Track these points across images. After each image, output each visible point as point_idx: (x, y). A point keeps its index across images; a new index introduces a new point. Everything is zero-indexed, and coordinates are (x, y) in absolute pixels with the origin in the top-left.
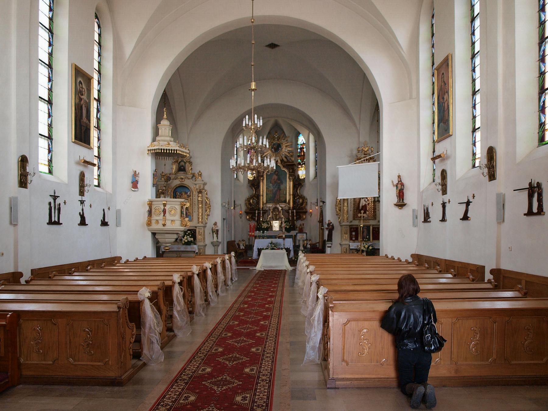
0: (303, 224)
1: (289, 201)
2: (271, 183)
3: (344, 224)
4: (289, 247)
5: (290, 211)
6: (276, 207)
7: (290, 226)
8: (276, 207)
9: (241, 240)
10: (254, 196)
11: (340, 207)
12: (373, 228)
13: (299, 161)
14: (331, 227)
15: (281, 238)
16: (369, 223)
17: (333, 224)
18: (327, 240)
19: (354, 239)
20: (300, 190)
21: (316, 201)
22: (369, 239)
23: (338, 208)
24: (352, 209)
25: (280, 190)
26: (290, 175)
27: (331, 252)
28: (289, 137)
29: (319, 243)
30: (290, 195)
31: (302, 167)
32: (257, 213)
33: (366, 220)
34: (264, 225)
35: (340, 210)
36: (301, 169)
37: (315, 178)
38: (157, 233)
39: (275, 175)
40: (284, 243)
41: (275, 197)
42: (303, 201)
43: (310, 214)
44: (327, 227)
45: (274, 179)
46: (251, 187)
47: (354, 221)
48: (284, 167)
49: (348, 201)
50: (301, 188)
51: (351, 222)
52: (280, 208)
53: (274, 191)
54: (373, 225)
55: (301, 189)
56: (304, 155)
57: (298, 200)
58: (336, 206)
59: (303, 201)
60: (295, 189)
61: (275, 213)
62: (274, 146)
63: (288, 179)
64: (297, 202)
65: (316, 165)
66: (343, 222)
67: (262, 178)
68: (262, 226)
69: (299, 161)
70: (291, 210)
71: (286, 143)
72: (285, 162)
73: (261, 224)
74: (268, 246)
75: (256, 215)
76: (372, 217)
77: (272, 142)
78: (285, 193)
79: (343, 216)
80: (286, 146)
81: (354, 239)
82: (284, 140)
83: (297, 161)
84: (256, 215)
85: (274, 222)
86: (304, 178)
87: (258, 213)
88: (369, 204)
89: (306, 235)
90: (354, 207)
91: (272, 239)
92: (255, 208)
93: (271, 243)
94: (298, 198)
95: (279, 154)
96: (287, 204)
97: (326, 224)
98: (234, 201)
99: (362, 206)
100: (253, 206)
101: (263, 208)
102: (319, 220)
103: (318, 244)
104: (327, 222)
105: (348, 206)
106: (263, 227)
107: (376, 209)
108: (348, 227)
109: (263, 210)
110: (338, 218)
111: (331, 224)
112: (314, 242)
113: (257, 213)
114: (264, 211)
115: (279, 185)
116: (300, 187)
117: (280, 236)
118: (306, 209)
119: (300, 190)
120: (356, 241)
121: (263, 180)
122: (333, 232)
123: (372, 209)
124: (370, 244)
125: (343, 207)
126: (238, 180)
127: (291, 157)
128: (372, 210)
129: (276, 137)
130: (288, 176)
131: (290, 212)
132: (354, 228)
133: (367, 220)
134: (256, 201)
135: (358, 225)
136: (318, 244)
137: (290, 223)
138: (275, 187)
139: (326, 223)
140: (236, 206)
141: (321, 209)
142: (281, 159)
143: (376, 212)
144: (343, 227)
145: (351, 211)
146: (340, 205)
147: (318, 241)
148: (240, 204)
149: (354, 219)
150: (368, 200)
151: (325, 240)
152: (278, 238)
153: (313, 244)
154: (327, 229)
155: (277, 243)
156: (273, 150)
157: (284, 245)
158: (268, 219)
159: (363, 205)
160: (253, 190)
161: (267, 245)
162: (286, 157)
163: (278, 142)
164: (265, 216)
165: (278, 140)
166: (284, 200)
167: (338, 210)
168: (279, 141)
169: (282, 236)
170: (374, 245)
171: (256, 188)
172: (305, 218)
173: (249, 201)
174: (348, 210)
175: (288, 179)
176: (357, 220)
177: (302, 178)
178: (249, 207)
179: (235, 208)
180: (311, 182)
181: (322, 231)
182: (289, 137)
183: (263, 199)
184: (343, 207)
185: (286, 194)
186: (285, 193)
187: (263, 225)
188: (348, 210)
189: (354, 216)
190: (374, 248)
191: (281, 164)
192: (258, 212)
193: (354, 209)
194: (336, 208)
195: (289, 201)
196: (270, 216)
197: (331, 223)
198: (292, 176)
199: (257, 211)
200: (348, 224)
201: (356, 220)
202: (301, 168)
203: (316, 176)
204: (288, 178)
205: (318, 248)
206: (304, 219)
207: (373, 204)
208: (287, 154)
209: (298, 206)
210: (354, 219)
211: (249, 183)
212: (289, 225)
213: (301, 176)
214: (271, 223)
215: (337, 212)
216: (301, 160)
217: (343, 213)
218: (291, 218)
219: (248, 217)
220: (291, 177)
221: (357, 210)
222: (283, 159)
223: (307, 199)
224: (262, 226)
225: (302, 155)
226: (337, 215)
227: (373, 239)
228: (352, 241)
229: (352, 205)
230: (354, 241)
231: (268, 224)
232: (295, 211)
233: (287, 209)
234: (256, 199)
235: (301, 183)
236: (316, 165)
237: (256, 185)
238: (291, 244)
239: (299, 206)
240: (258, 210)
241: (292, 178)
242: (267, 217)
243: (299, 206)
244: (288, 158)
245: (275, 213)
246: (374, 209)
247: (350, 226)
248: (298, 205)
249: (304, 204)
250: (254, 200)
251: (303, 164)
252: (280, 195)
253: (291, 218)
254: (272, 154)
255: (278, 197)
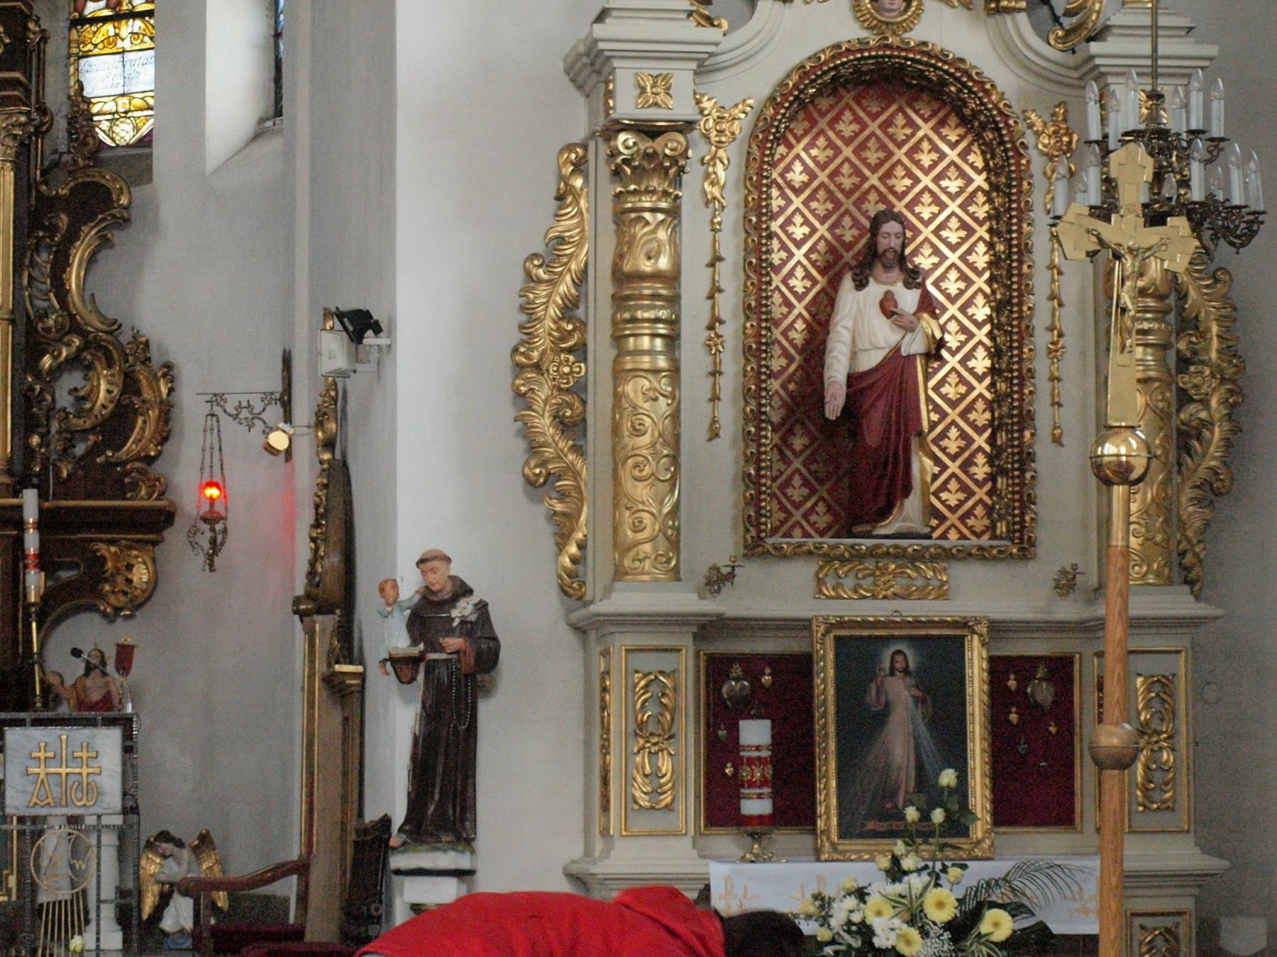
0: (125, 656)
3: (625, 600)
11: (579, 389)
12: (998, 668)
14: (453, 643)
16: (942, 595)
17: (482, 607)
18: (399, 818)
19: (756, 805)
21: (277, 387)
22: (958, 825)
23: (543, 392)
24: (729, 414)
29: (301, 868)
33: (899, 555)
35: (573, 427)
36: (111, 41)
37: (259, 134)
38: (609, 817)
42: (130, 385)
43: (204, 541)
44: (400, 642)
47: (749, 572)
49: (674, 301)
50: (105, 242)
51: (717, 580)
54: (998, 629)
55: (104, 255)
57: (72, 379)
58: (520, 368)
59: (130, 385)
60: (44, 258)
64: (64, 400)
66: (619, 573)
76: (978, 522)
79: (618, 498)
81: (756, 805)
86: (146, 142)
88: (935, 351)
90: (754, 391)
94: (75, 361)
97: (393, 601)
99: (852, 379)
104: (409, 586)
105: (675, 371)
107: (1025, 419)
108: (686, 642)
110: (545, 532)
111: (464, 609)
112: (244, 864)
116: (89, 234)
120: (783, 838)
122: (487, 710)
123: (982, 417)
124: (979, 871)
125: (619, 374)
128: (981, 441)
132: (752, 664)
133: (918, 556)
135: (804, 626)
136: (288, 887)
139: (388, 588)
141: (329, 444)
143: (1026, 458)
144: (622, 641)
145: (714, 435)
146: (580, 351)
147: (294, 852)
149: (755, 548)
150: (928, 305)
151: (386, 822)
154: (402, 666)
159: (870, 360)
167: (544, 424)
170: (1031, 890)
172: (154, 583)
174: (675, 416)
176: (799, 553)
177: (125, 133)
181: (336, 719)
184: (619, 374)
188: (675, 416)
189: (755, 501)
190: (1042, 928)
193: (757, 417)
194: (522, 399)
197: (463, 590)
200: (686, 601)
201: (779, 554)
202: (109, 28)
203: (278, 112)
205: (298, 933)
206: (138, 603)
207: (981, 363)
209: (69, 444)
210: (755, 548)
213: (115, 117)
215: (534, 448)
217: (618, 457)
221: (786, 430)
223: (169, 369)
226: (531, 483)
227: (1005, 814)
228: (726, 841)
229: (731, 365)
230: (756, 829)
235: (108, 192)
239: (80, 449)
246: (995, 426)
247: (707, 628)
248: (71, 437)
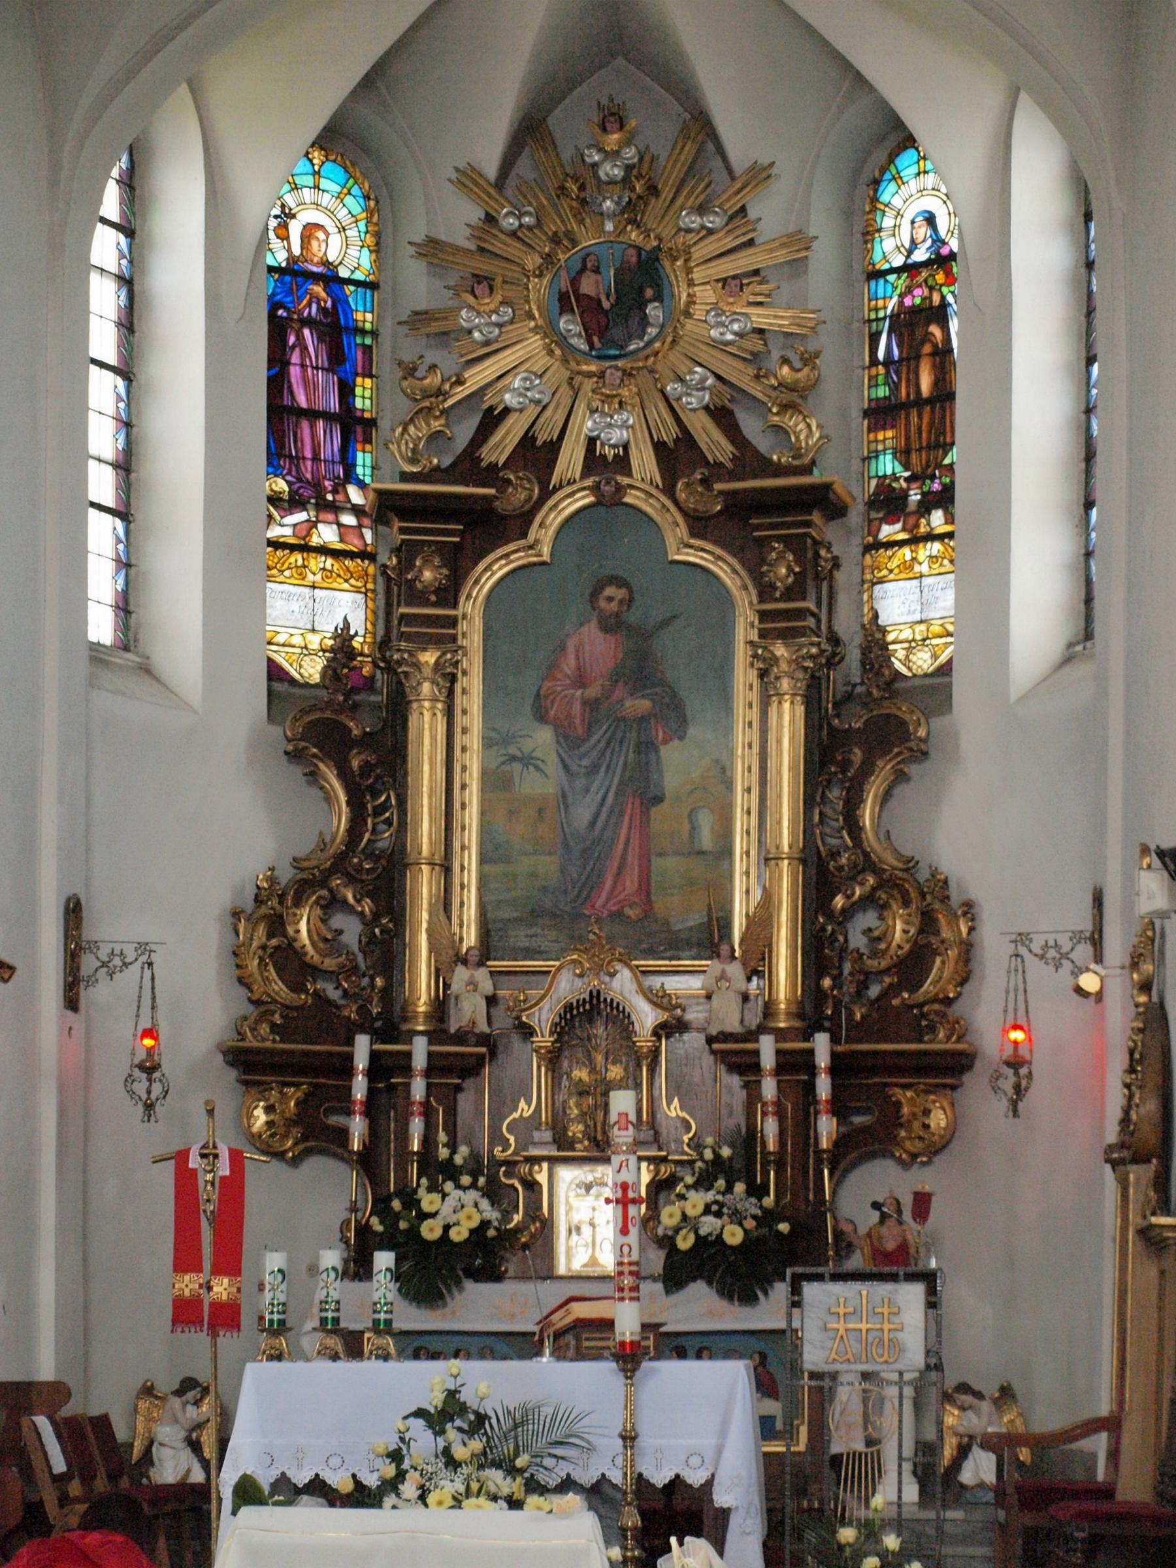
0: (922, 1203)
1: (761, 922)
2: (541, 716)
4: (695, 1478)
5: (767, 1049)
6: (595, 997)
7: (767, 1218)
8: (595, 997)
9: (166, 1383)
10: (340, 864)
13: (887, 465)
15: (595, 1355)
20: (886, 797)
21: (1087, 926)
25: (658, 799)
26: (763, 616)
27: (654, 1279)
28: (760, 174)
29: (1112, 1424)
30: (769, 859)
31: (915, 540)
32: (361, 1061)
34: (447, 1209)
37: (1067, 660)
39: (591, 631)
40: (631, 1405)
41: (591, 884)
42: (928, 922)
43: (1008, 1085)
45: (581, 680)
46: (295, 756)
48: (699, 525)
50: (901, 776)
52: (646, 1017)
53: (582, 814)
55: (901, 790)
56: (944, 395)
57: (868, 919)
59: (928, 922)
61: (581, 1074)
62: (588, 286)
63: (744, 676)
64: (857, 941)
65: (1090, 360)
67: (429, 657)
68: (424, 1216)
69: (887, 465)
70: (780, 1035)
71: (729, 242)
72: (716, 470)
73: (411, 1201)
74: (396, 1456)
75: (359, 1088)
77: (555, 240)
78: (706, 840)
80: (731, 284)
82: (701, 210)
83: (863, 477)
84: (359, 1088)
85: (567, 1175)
86: (945, 670)
87: (379, 1068)
89: (932, 1303)
91: (454, 1365)
92: (351, 1012)
93: (437, 1420)
94: (868, 901)
95: (644, 379)
96: (735, 970)
98: (73, 911)
100: (333, 994)
101: (440, 1008)
102: (1112, 1134)
103: (1099, 1443)
106: (430, 1231)
109: (436, 1035)
113: (361, 1061)
114: (460, 1038)
115: (647, 748)
117: (582, 1325)
118: (959, 1030)
119: (886, 797)
121: (449, 679)
126: (146, 670)
127: (785, 407)
129: (612, 171)
130: (745, 628)
131: (768, 1060)
134: (369, 923)
136: (1099, 1443)
137: (757, 1191)
138: (594, 768)
140: (88, 963)
142: (669, 433)
147: (1104, 1408)
148: (143, 947)
152: (559, 1354)
153: (1041, 1443)
155: (521, 1420)
156: (569, 325)
157: (629, 1438)
158: (497, 1138)
160: (329, 798)
161: (393, 1443)
162: (722, 415)
163: (634, 235)
164: (464, 1102)
165: (631, 213)
166: (696, 918)
168: (650, 221)
169: (607, 1325)
171: (366, 768)
173: (277, 924)
175: (744, 676)
177: (923, 661)
178: (279, 988)
179: (87, 996)
180: (1023, 698)
182: (760, 174)
183: (445, 903)
185: (726, 852)
186: (706, 840)
187: (429, 1201)
191: (669, 490)
192: (374, 1056)
195: (761, 922)
196: (524, 1109)
198: (786, 635)
199: (362, 1047)
202: (906, 553)
203: (1088, 635)
204: (741, 655)
205: (1107, 1492)
206: (936, 1148)
208: (741, 375)
209: (863, 986)
211: (272, 716)
212: (751, 1207)
213: (912, 645)
214: (531, 1186)
216: (903, 455)
218: (770, 1128)
219: (260, 1118)
220: (780, 650)
222: (686, 439)
223: (969, 909)
224: (424, 1216)
225: (919, 402)
231: (494, 1193)
232: (821, 1044)
233: (733, 1024)
234: (367, 906)
235: (903, 723)
236: (1089, 505)
237: (366, 741)
238: (723, 1433)
239: (874, 991)
240: (380, 1035)
241: (797, 663)
242: (497, 1117)
243: (874, 991)
244: (750, 426)
245: (581, 1074)
248: (865, 978)
249: (941, 971)
250: (339, 920)
251: (926, 507)
252: (645, 859)
253: (770, 1128)
254: (556, 373)
255: (631, 883)
